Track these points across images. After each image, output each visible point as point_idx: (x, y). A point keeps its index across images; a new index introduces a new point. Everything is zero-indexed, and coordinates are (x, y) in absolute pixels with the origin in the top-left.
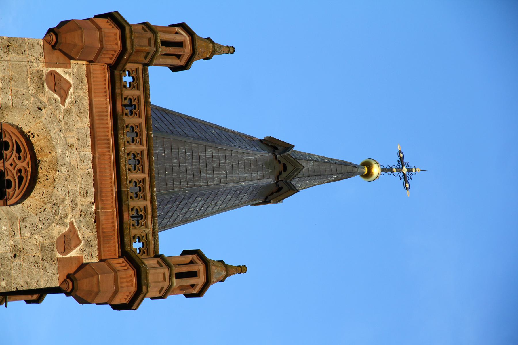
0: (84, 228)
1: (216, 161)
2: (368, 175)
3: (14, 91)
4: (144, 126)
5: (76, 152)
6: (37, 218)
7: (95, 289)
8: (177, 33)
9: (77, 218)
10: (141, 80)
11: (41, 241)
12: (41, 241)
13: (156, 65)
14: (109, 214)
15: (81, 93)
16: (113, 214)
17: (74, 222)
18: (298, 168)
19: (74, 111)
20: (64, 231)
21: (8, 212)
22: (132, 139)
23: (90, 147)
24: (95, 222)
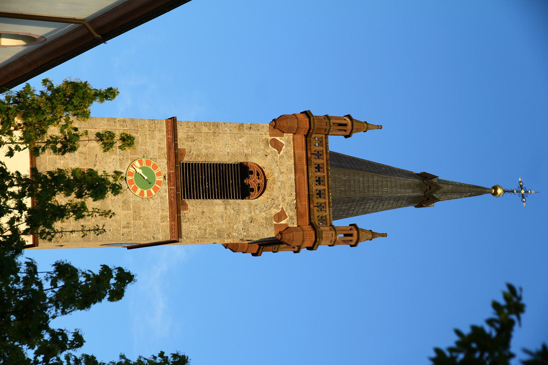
0: (289, 211)
1: (380, 183)
2: (495, 194)
3: (252, 148)
4: (325, 164)
5: (285, 176)
6: (263, 205)
7: (292, 239)
8: (344, 120)
9: (285, 206)
10: (324, 142)
11: (266, 215)
12: (266, 215)
13: (330, 135)
14: (303, 205)
15: (289, 148)
16: (306, 205)
17: (284, 208)
18: (438, 188)
19: (285, 156)
20: (278, 212)
21: (249, 202)
22: (134, 142)
23: (294, 173)
24: (295, 208)
